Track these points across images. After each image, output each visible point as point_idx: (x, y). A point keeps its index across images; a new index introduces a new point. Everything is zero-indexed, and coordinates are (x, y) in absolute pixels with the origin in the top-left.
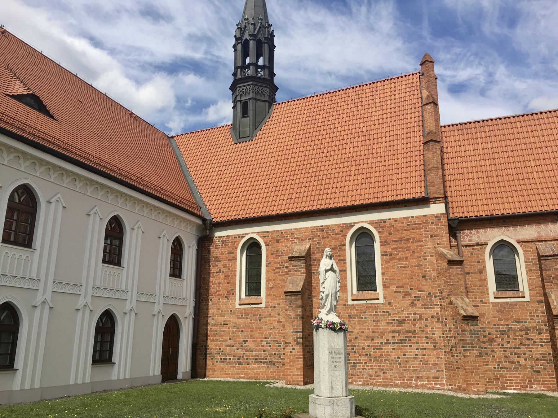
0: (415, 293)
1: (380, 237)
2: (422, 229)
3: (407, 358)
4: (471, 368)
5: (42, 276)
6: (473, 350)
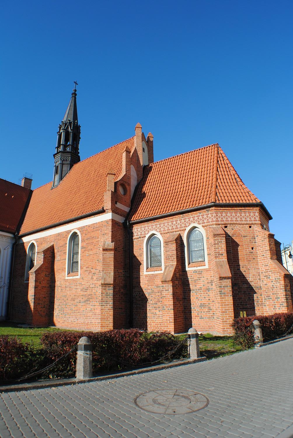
0: (93, 271)
1: (81, 237)
4: (104, 317)
5: (3, 276)
6: (107, 305)
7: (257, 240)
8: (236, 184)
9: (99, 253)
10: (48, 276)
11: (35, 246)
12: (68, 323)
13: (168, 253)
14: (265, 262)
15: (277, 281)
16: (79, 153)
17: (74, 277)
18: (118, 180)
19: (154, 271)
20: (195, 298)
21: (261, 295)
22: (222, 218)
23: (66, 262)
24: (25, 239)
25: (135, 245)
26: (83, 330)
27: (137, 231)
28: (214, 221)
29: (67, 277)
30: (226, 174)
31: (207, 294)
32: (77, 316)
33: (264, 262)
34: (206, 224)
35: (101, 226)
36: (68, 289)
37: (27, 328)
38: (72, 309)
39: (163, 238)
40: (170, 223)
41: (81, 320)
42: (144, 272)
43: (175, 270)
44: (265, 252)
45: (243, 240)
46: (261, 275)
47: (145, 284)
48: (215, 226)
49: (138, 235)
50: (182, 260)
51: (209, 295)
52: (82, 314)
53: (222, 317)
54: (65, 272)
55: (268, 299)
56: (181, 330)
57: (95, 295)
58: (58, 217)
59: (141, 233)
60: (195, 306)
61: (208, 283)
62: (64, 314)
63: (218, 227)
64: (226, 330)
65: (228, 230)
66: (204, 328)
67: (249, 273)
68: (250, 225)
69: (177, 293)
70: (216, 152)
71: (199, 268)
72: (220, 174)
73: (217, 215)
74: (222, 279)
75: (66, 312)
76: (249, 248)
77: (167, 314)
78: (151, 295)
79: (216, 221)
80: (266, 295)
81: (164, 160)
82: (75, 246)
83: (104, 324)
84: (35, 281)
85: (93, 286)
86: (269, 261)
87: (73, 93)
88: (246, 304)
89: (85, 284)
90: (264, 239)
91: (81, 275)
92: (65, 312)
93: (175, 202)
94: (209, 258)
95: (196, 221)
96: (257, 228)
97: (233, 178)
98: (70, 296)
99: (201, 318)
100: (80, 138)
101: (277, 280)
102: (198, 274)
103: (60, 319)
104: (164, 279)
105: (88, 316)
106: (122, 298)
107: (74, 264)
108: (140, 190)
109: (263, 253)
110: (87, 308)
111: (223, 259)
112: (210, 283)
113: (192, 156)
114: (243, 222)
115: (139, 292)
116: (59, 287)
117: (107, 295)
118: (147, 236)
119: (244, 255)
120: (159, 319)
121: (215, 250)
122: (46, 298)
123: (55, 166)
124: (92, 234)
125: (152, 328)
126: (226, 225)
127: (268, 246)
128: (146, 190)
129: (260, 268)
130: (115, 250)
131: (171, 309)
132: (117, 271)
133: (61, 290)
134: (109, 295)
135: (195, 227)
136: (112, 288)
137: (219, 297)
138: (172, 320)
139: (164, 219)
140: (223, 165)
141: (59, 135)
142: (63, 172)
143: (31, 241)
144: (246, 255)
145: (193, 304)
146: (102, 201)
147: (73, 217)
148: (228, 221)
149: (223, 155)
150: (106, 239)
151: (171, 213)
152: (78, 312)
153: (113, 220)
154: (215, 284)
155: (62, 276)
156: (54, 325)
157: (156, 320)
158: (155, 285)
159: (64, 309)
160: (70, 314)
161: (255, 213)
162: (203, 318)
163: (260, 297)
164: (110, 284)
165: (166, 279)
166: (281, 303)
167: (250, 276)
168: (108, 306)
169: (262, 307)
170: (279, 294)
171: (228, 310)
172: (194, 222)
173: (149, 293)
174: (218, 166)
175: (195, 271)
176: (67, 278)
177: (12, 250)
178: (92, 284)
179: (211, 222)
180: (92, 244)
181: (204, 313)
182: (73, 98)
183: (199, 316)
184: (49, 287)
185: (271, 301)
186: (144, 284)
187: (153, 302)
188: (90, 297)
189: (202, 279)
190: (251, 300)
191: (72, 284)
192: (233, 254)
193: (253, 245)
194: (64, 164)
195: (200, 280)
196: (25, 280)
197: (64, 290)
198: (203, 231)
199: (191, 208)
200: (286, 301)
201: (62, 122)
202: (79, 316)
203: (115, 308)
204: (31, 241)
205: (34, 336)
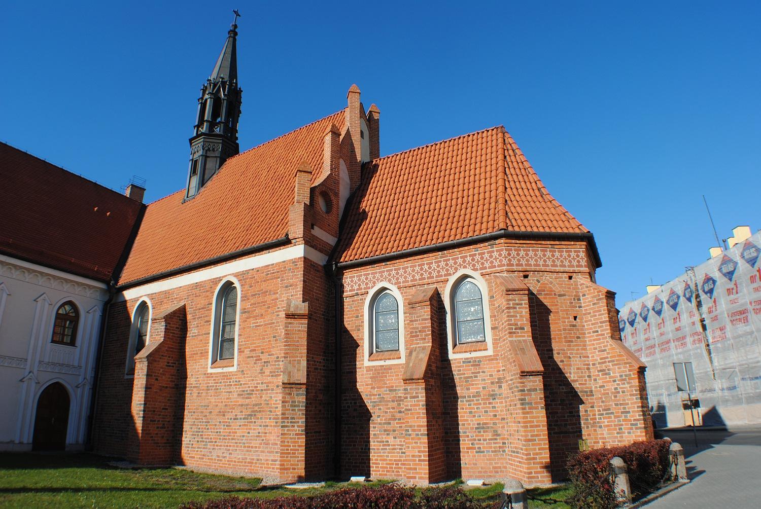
0: (265, 357)
1: (242, 291)
2: (279, 278)
3: (251, 436)
5: (83, 365)
6: (293, 426)
7: (584, 303)
8: (540, 199)
9: (278, 322)
10: (173, 366)
11: (147, 307)
12: (212, 459)
13: (415, 324)
14: (599, 343)
15: (625, 380)
16: (237, 138)
17: (226, 370)
18: (316, 184)
20: (466, 413)
21: (592, 407)
22: (519, 260)
23: (209, 340)
24: (129, 294)
25: (347, 308)
26: (242, 475)
27: (352, 281)
28: (504, 265)
29: (212, 368)
30: (521, 179)
31: (491, 406)
32: (230, 446)
33: (597, 344)
34: (488, 270)
35: (282, 271)
36: (211, 392)
37: (127, 469)
38: (220, 432)
39: (403, 296)
40: (417, 268)
41: (238, 455)
42: (364, 362)
43: (430, 358)
44: (600, 325)
45: (557, 302)
46: (593, 368)
47: (367, 385)
48: (505, 274)
49: (354, 290)
50: (440, 338)
51: (495, 407)
52: (240, 443)
53: (526, 450)
54: (207, 358)
55: (606, 414)
56: (441, 474)
57: (268, 404)
58: (196, 253)
59: (359, 285)
60: (467, 428)
61: (492, 383)
62: (203, 441)
63: (511, 277)
64: (533, 475)
65: (530, 283)
66: (486, 472)
67: (570, 365)
68: (571, 275)
69: (432, 402)
70: (500, 140)
71: (474, 354)
72: (510, 178)
73: (509, 255)
74: (526, 375)
75: (208, 438)
76: (569, 318)
77: (414, 445)
78: (378, 405)
79: (508, 265)
80: (601, 406)
81: (401, 154)
82: (229, 310)
83: (288, 465)
84: (147, 375)
85: (264, 387)
86: (607, 342)
87: (231, 31)
88: (566, 425)
89: (247, 384)
90: (597, 300)
91: (239, 365)
92: (205, 438)
93: (427, 229)
94: (494, 335)
95: (469, 263)
96: (582, 280)
97: (535, 187)
98: (217, 406)
99: (479, 452)
100: (240, 112)
101: (624, 377)
102: (472, 366)
103: (194, 451)
104: (408, 374)
105: (252, 447)
106: (320, 411)
107: (225, 344)
108: (356, 207)
109: (595, 328)
110: (251, 431)
111: (524, 336)
112: (497, 383)
113: (456, 147)
114: (558, 269)
115: (353, 399)
116: (194, 387)
117: (295, 406)
118: (372, 292)
119: (560, 331)
120: (394, 453)
121: (509, 320)
122: (167, 409)
123: (192, 159)
124: (264, 286)
125: (379, 471)
126: (527, 273)
127: (605, 314)
128: (368, 207)
129: (590, 356)
130: (310, 316)
131: (421, 435)
132: (313, 358)
133: (199, 393)
134: (299, 406)
135: (385, 289)
136: (303, 391)
137: (520, 411)
138: (425, 456)
139: (406, 260)
140: (515, 164)
141: (201, 103)
142: (207, 171)
143: (141, 297)
144: (565, 330)
145: (463, 425)
146: (284, 222)
147: (226, 253)
148: (530, 265)
149: (514, 146)
150: (292, 296)
151: (420, 248)
152: (232, 439)
153: (306, 260)
154: (509, 385)
155: (200, 368)
156: (182, 463)
157: (388, 456)
158: (387, 387)
159: (202, 432)
160: (216, 442)
161: (579, 252)
162: (483, 452)
163: (591, 411)
164: (301, 384)
165: (412, 374)
166: (633, 422)
167: (572, 371)
168: (296, 428)
169: (595, 430)
170: (628, 404)
171: (537, 435)
172: (465, 267)
173: (375, 402)
174: (506, 166)
175: (467, 361)
176: (210, 371)
177: (103, 313)
178: (262, 383)
179: (499, 266)
180: (264, 305)
181: (485, 442)
182: (231, 39)
183: (475, 448)
184: (173, 388)
185: (613, 419)
186: (364, 384)
187: (381, 420)
188: (256, 408)
189: (480, 376)
190: (574, 416)
191: (221, 383)
192: (539, 327)
193: (576, 311)
194: (209, 157)
195: (476, 377)
196: (126, 372)
197: (204, 394)
198: (481, 287)
199: (459, 239)
200: (642, 417)
201: (208, 80)
202: (234, 446)
203: (309, 431)
204: (141, 297)
205: (145, 489)
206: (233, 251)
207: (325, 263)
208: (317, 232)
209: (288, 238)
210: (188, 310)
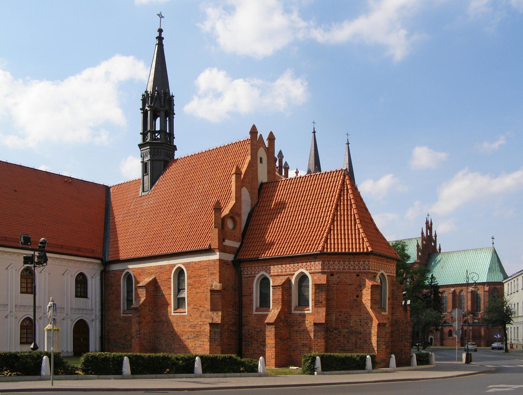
0: (202, 309)
5: (94, 308)
19: (263, 311)
85: (202, 323)
95: (304, 266)
100: (174, 138)
172: (302, 268)
206: (180, 250)
207: (233, 259)
208: (228, 243)
209: (210, 248)
210: (157, 278)
